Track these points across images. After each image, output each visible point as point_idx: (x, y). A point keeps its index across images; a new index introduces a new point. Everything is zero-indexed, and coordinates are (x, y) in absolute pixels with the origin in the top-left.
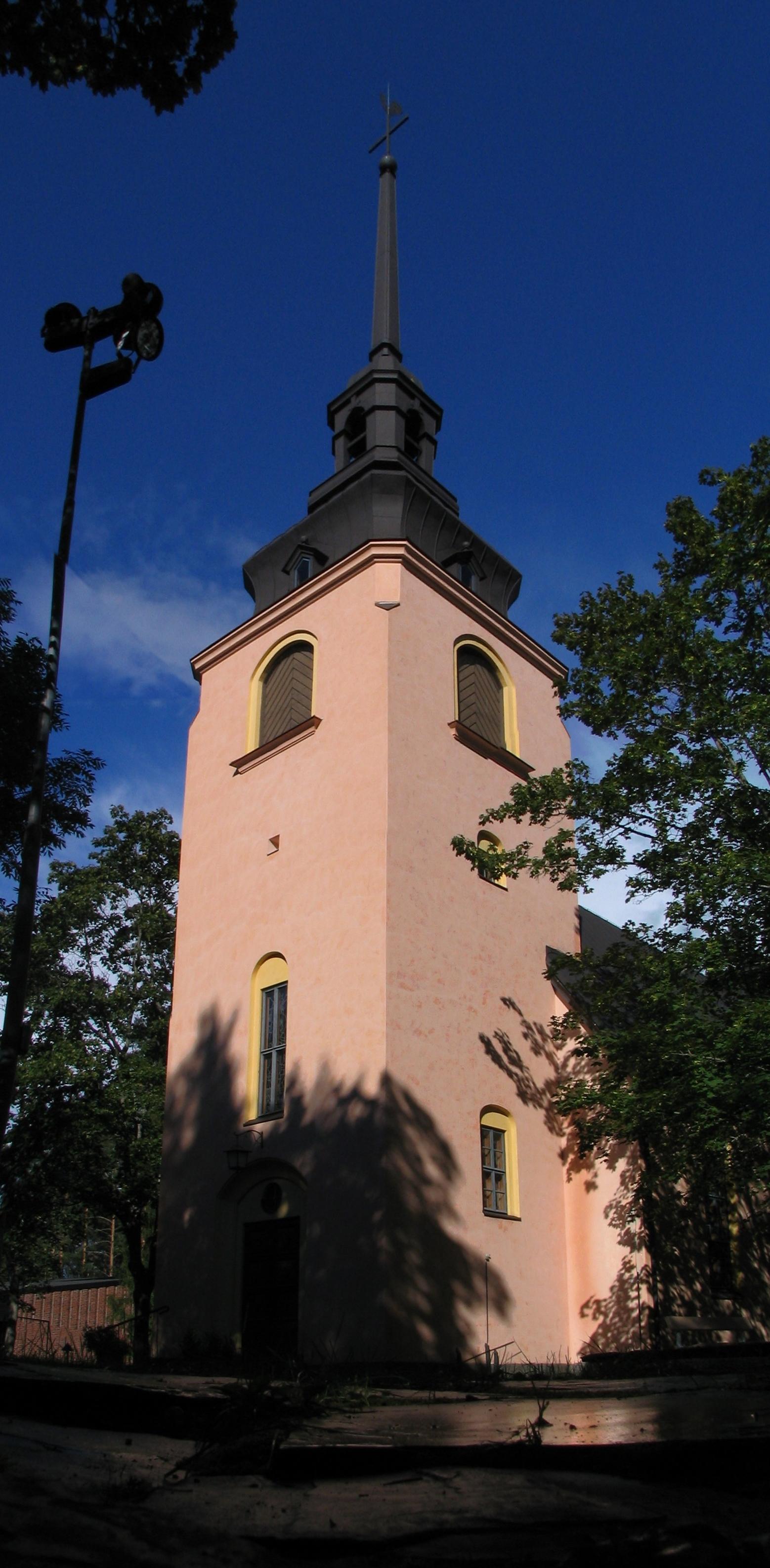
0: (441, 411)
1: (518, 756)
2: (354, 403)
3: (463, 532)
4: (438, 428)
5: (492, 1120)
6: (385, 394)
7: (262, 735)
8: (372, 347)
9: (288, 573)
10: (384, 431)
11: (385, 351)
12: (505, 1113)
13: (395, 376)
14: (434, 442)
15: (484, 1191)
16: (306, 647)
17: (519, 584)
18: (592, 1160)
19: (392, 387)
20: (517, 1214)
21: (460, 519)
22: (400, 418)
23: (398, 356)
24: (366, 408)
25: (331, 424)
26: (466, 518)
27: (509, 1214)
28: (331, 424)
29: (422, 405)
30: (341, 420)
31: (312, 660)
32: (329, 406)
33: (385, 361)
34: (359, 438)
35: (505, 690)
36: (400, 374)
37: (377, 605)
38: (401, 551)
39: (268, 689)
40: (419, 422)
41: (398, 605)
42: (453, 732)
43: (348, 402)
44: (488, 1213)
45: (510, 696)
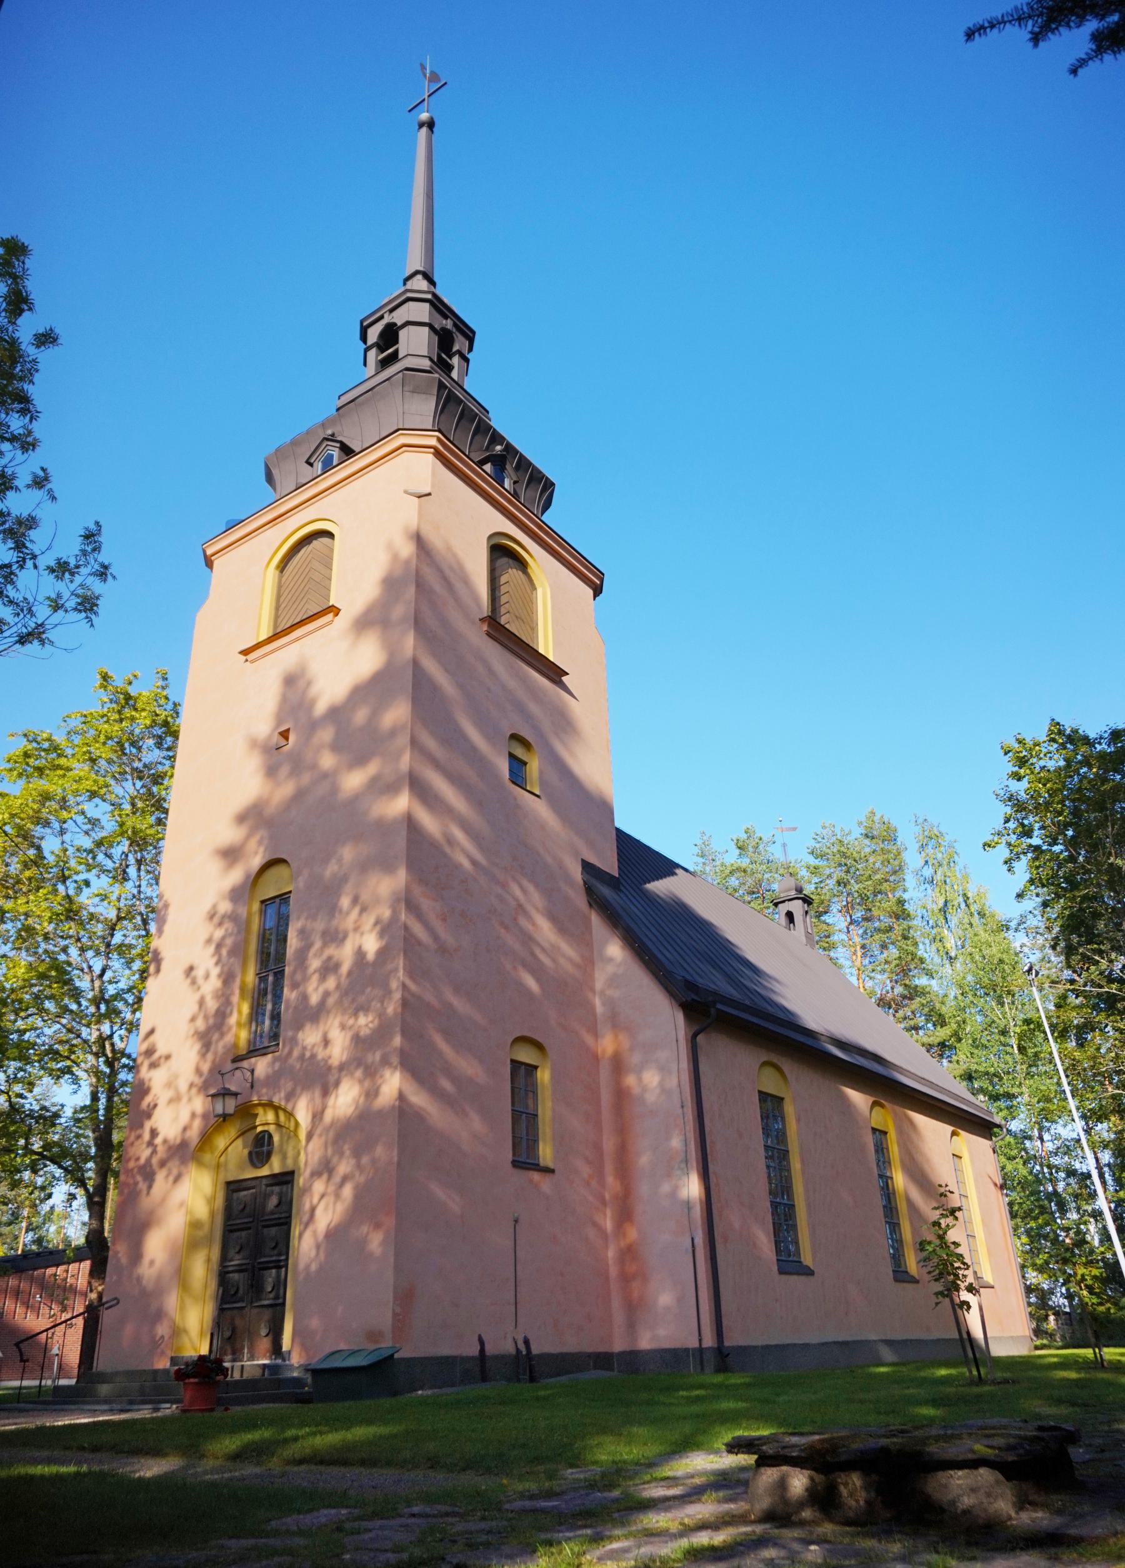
0: (474, 333)
1: (551, 659)
2: (387, 319)
3: (497, 438)
4: (470, 349)
5: (526, 1055)
6: (421, 312)
7: (275, 626)
8: (407, 274)
9: (311, 465)
10: (416, 344)
11: (419, 277)
12: (539, 1046)
13: (429, 296)
14: (467, 360)
15: (514, 1137)
16: (329, 535)
17: (553, 491)
18: (253, 844)
19: (427, 305)
20: (551, 1165)
21: (492, 423)
22: (432, 334)
23: (432, 283)
24: (399, 324)
25: (364, 338)
26: (498, 422)
27: (542, 1163)
28: (364, 338)
29: (455, 325)
30: (373, 334)
31: (332, 550)
32: (362, 322)
33: (420, 283)
34: (390, 351)
35: (540, 591)
36: (434, 295)
37: (406, 492)
38: (433, 442)
39: (284, 579)
40: (452, 336)
41: (429, 494)
42: (485, 627)
43: (382, 317)
44: (516, 1164)
45: (543, 597)
